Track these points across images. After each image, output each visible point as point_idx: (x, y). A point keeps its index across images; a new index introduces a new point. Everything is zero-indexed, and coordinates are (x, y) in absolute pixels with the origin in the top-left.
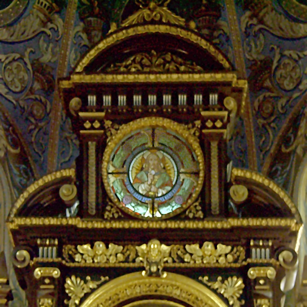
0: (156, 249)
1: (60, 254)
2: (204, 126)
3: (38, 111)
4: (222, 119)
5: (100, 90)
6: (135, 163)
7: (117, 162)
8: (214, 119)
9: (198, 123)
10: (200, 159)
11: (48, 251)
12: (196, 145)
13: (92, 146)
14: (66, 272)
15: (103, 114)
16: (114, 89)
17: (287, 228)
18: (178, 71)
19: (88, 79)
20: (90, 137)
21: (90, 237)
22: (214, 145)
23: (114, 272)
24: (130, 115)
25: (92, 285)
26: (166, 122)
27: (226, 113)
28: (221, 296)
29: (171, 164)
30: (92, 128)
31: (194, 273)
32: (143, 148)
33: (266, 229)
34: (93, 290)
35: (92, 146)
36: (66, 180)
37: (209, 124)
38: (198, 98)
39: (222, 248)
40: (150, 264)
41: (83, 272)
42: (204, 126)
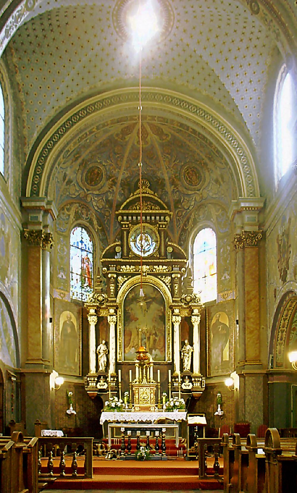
0: (145, 268)
1: (116, 270)
2: (159, 227)
3: (107, 214)
4: (165, 224)
5: (128, 215)
6: (139, 238)
7: (133, 237)
8: (162, 225)
9: (158, 225)
10: (158, 235)
11: (113, 269)
12: (157, 233)
13: (125, 233)
14: (118, 275)
15: (128, 223)
16: (132, 215)
17: (184, 262)
18: (151, 209)
19: (124, 212)
20: (125, 230)
21: (125, 264)
22: (162, 233)
23: (133, 275)
24: (137, 223)
25: (126, 279)
26: (148, 225)
27: (166, 223)
28: (164, 282)
29: (149, 238)
30: (125, 227)
31: (156, 275)
32: (141, 233)
33: (178, 262)
34: (126, 281)
35: (125, 233)
36: (117, 245)
37: (161, 226)
38: (158, 218)
39: (165, 267)
40: (143, 272)
41: (123, 275)
42: (159, 227)
